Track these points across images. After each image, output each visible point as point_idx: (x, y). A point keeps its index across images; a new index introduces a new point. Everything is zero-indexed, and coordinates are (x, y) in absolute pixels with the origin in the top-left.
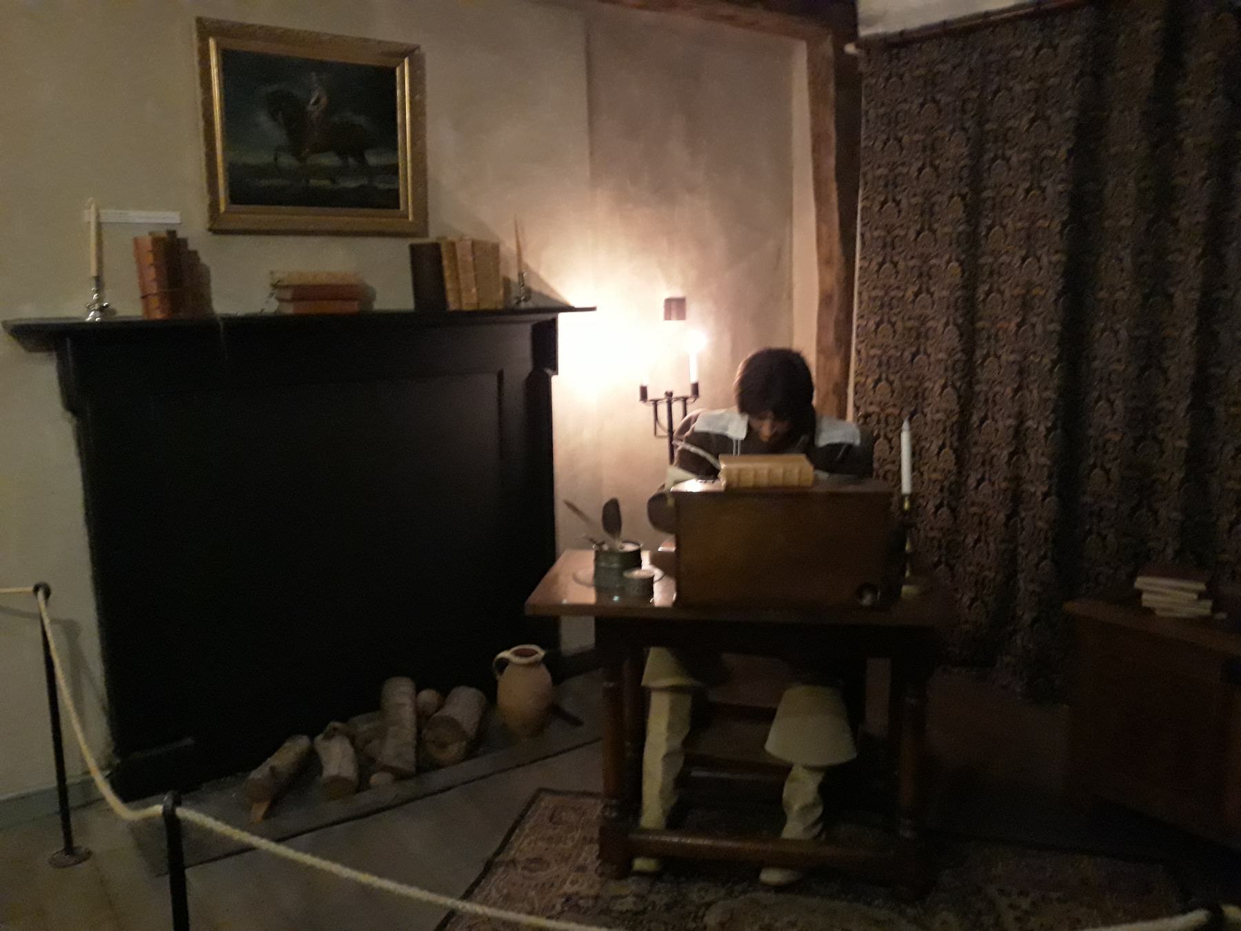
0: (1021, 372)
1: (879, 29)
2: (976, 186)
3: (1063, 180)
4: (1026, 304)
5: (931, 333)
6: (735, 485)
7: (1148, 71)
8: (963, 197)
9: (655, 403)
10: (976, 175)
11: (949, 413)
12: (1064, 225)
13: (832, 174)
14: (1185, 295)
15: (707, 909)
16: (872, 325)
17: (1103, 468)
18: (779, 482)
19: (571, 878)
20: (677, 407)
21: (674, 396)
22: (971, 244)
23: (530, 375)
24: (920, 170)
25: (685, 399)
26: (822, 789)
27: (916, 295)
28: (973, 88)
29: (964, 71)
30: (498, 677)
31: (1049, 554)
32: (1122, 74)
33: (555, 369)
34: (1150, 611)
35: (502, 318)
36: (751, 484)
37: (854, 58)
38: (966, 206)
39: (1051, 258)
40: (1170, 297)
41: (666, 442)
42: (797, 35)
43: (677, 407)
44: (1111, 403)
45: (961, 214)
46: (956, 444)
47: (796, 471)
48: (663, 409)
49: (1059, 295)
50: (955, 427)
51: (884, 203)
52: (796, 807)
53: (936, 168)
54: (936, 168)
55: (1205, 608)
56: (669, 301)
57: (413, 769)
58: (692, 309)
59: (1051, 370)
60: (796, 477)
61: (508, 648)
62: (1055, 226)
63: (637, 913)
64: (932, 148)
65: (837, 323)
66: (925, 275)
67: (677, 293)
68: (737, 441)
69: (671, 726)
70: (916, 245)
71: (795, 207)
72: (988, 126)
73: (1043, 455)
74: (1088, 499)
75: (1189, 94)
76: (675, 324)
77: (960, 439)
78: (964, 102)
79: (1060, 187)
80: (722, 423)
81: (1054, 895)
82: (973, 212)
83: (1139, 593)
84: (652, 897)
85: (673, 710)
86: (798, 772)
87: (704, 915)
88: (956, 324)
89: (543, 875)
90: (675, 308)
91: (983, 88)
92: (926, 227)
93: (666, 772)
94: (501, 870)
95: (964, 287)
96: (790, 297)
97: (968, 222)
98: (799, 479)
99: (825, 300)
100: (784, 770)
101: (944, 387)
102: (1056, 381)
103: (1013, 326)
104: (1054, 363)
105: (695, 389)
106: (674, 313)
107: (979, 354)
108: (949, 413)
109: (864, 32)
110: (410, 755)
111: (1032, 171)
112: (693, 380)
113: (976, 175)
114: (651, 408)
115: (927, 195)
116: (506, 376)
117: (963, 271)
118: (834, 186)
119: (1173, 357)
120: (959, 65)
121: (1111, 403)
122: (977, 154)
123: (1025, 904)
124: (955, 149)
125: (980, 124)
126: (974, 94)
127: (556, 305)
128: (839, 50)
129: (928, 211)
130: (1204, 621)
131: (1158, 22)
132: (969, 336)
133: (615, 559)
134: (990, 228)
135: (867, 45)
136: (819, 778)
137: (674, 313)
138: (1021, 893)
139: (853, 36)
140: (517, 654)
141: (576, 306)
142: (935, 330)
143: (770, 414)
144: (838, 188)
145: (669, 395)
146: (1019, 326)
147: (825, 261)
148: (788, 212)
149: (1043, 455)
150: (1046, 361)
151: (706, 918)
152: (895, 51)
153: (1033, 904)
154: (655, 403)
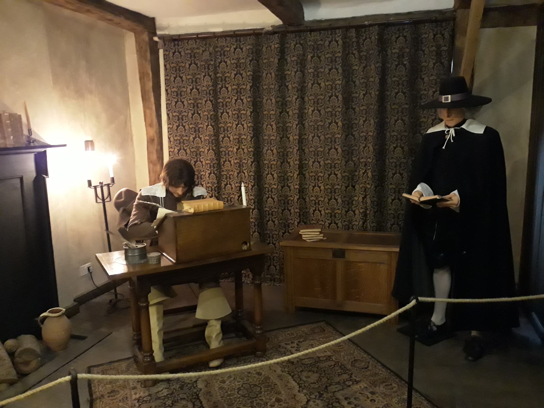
0: (240, 166)
1: (166, 32)
2: (216, 97)
3: (249, 97)
4: (240, 141)
5: (202, 153)
6: (197, 212)
7: (276, 61)
8: (211, 101)
9: (95, 188)
10: (215, 93)
11: (213, 183)
12: (251, 113)
13: (151, 90)
14: (293, 137)
15: (196, 383)
16: (176, 151)
17: (272, 198)
18: (212, 209)
19: (133, 393)
20: (105, 189)
21: (104, 184)
22: (215, 119)
23: (36, 178)
24: (191, 90)
25: (108, 185)
26: (222, 326)
27: (194, 139)
28: (212, 60)
29: (207, 53)
30: (42, 326)
31: (256, 230)
32: (265, 61)
33: (47, 174)
34: (305, 240)
35: (18, 151)
36: (202, 211)
37: (156, 42)
38: (213, 105)
39: (248, 123)
40: (288, 138)
41: (102, 205)
42: (132, 30)
43: (105, 189)
44: (273, 175)
45: (211, 108)
46: (217, 195)
47: (207, 205)
48: (99, 190)
49: (252, 138)
50: (216, 188)
51: (176, 102)
52: (214, 336)
53: (198, 90)
54: (198, 90)
55: (321, 237)
56: (87, 142)
57: (16, 378)
58: (96, 145)
59: (251, 165)
60: (207, 207)
61: (45, 311)
62: (249, 113)
63: (171, 394)
64: (195, 81)
65: (157, 151)
66: (197, 131)
67: (90, 139)
68: (161, 198)
69: (158, 319)
70: (280, 118)
71: (130, 102)
72: (218, 75)
73: (251, 195)
74: (267, 209)
75: (289, 70)
76: (90, 151)
77: (218, 193)
78: (209, 65)
79: (248, 100)
80: (153, 191)
81: (301, 340)
82: (215, 107)
83: (301, 235)
84: (172, 388)
85: (158, 313)
86: (213, 323)
87: (197, 386)
88: (213, 150)
89: (119, 396)
90: (89, 144)
91: (215, 60)
92: (196, 112)
93: (159, 338)
94: (98, 401)
95: (215, 135)
96: (132, 140)
97: (214, 111)
98: (214, 206)
99: (150, 141)
100: (204, 324)
101: (210, 174)
102: (253, 169)
103: (235, 150)
104: (252, 162)
105: (113, 180)
106: (90, 148)
107: (222, 160)
108: (213, 183)
109: (159, 33)
110: (14, 372)
111: (237, 93)
112: (112, 176)
113: (215, 93)
114: (93, 190)
115: (195, 99)
116: (24, 179)
117: (214, 129)
118: (152, 94)
119: (291, 158)
120: (205, 50)
121: (273, 175)
122: (215, 85)
123: (295, 345)
124: (206, 83)
125: (215, 74)
126: (212, 63)
127: (44, 144)
128: (151, 39)
129: (196, 105)
130: (321, 240)
131: (278, 45)
132: (218, 154)
133: (136, 251)
134: (222, 113)
135: (162, 37)
136: (220, 322)
137: (90, 148)
138: (292, 343)
139: (155, 34)
140: (51, 312)
141: (52, 144)
142: (204, 152)
143: (183, 185)
144: (154, 95)
145: (101, 183)
146: (237, 149)
147: (149, 125)
148: (127, 103)
149: (251, 195)
150: (249, 161)
151: (198, 386)
152: (176, 42)
153: (297, 345)
154: (95, 188)
